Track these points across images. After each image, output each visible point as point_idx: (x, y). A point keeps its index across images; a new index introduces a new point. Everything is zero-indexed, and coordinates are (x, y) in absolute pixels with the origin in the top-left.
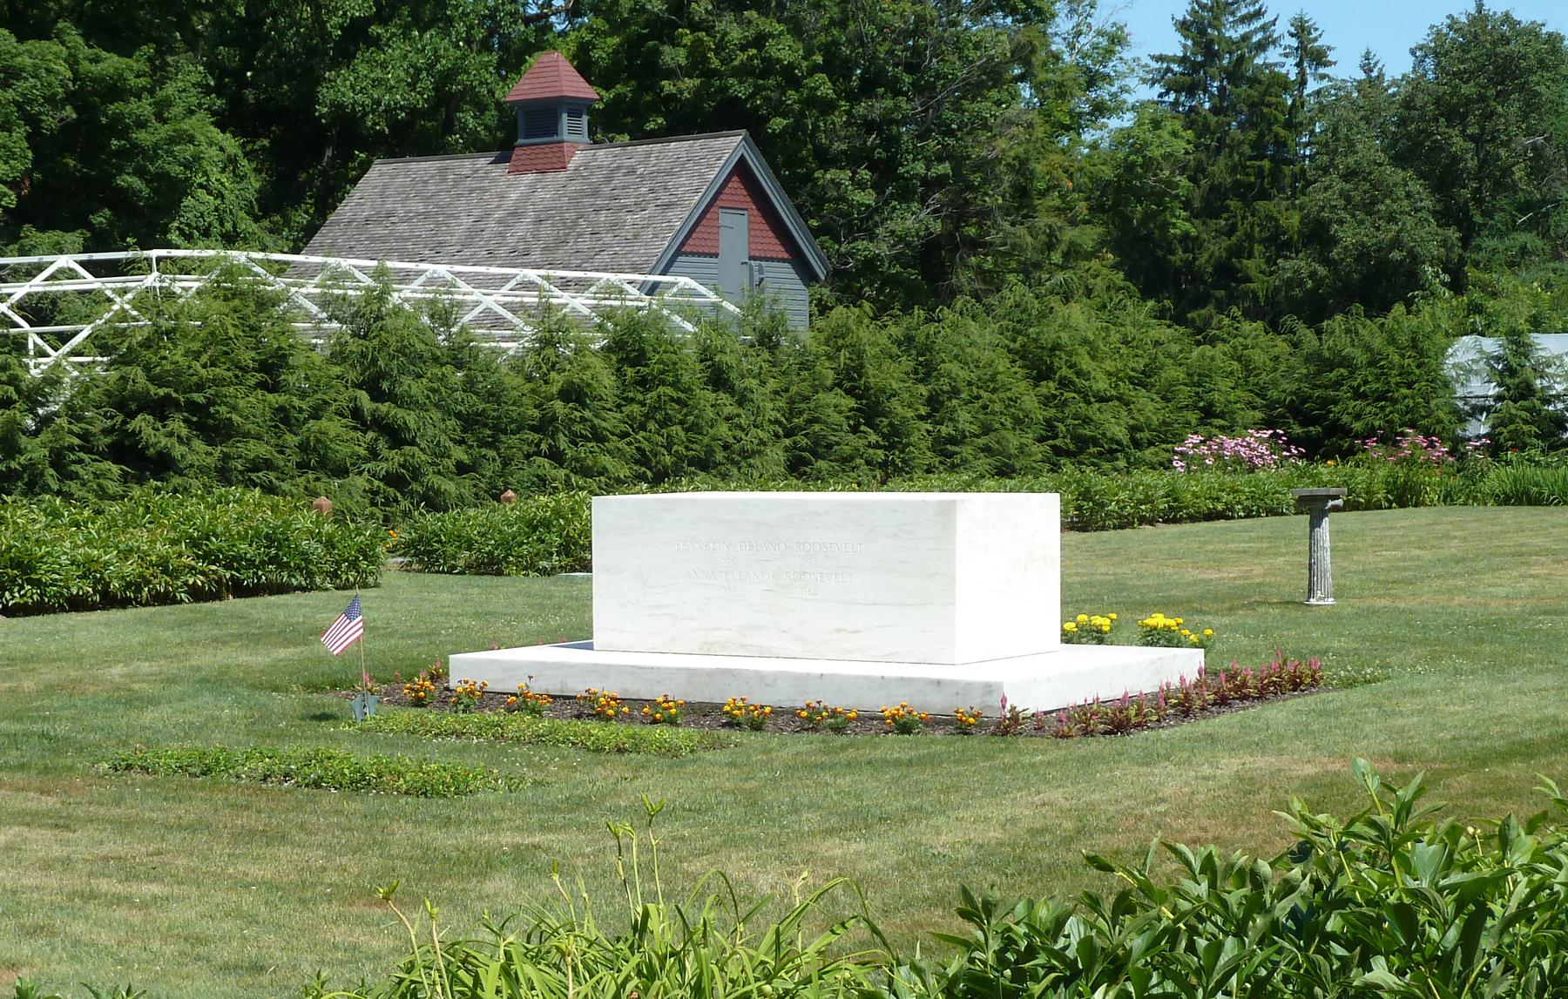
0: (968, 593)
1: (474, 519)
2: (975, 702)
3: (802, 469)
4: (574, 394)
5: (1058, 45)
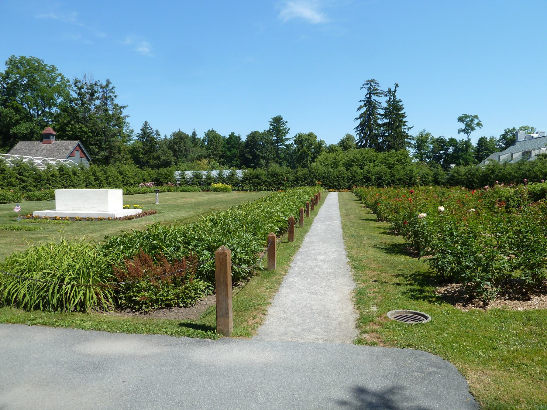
0: (110, 202)
1: (37, 193)
2: (111, 216)
3: (87, 187)
4: (52, 176)
5: (124, 131)
